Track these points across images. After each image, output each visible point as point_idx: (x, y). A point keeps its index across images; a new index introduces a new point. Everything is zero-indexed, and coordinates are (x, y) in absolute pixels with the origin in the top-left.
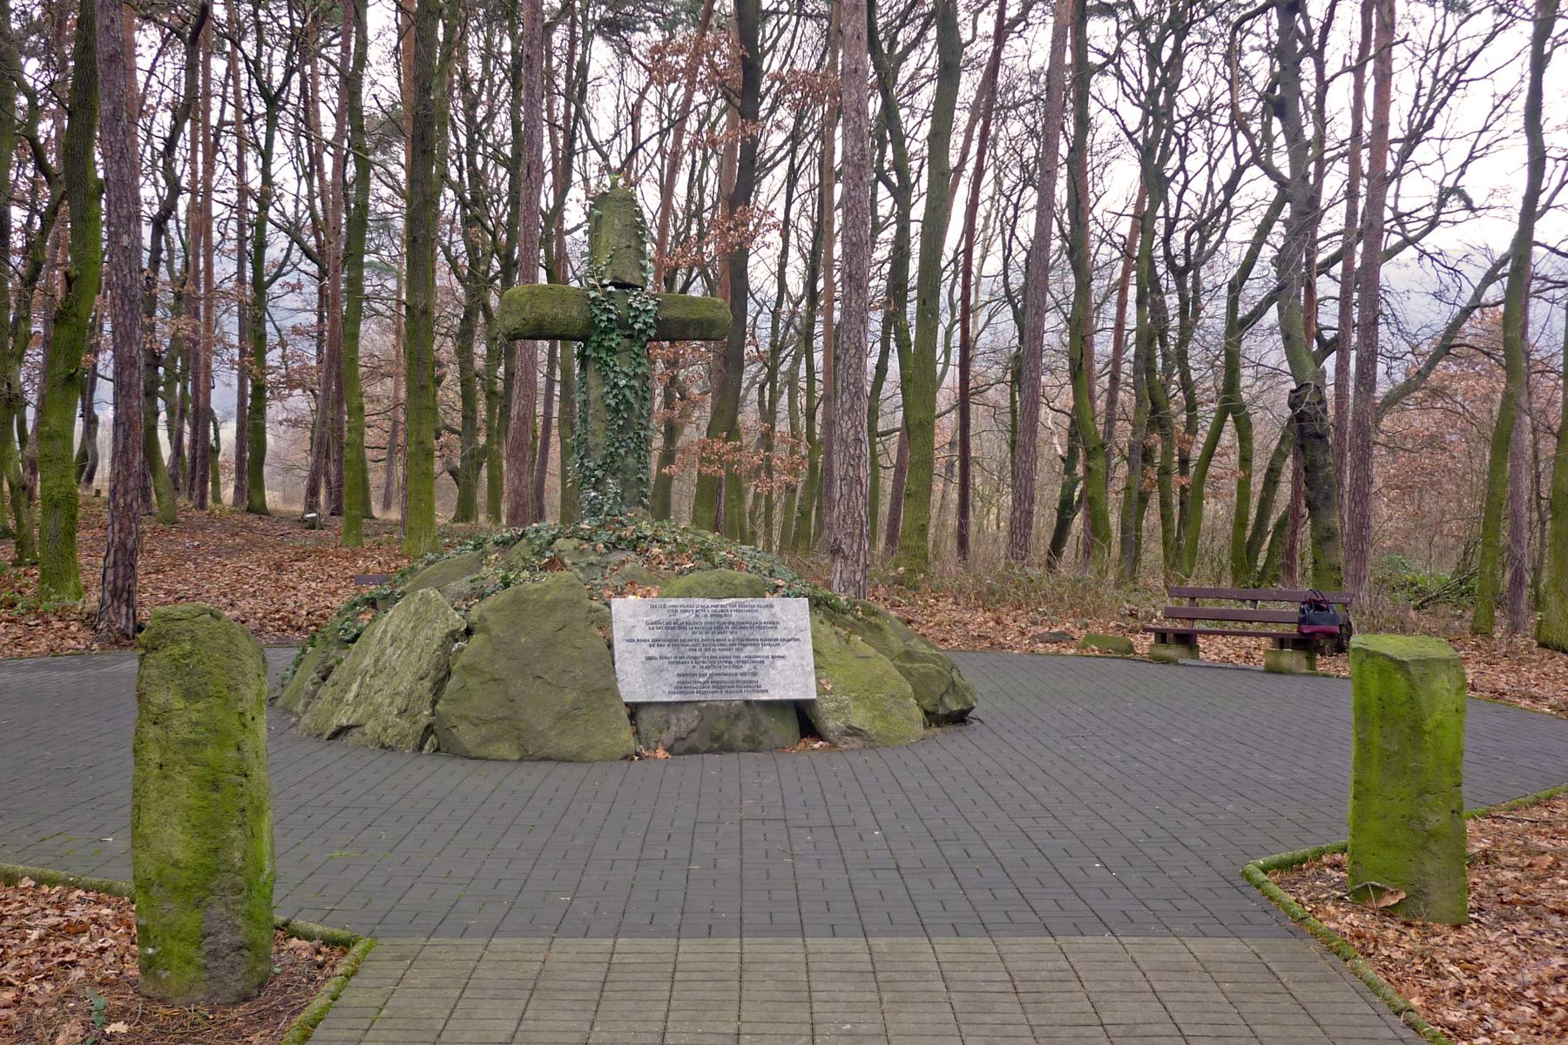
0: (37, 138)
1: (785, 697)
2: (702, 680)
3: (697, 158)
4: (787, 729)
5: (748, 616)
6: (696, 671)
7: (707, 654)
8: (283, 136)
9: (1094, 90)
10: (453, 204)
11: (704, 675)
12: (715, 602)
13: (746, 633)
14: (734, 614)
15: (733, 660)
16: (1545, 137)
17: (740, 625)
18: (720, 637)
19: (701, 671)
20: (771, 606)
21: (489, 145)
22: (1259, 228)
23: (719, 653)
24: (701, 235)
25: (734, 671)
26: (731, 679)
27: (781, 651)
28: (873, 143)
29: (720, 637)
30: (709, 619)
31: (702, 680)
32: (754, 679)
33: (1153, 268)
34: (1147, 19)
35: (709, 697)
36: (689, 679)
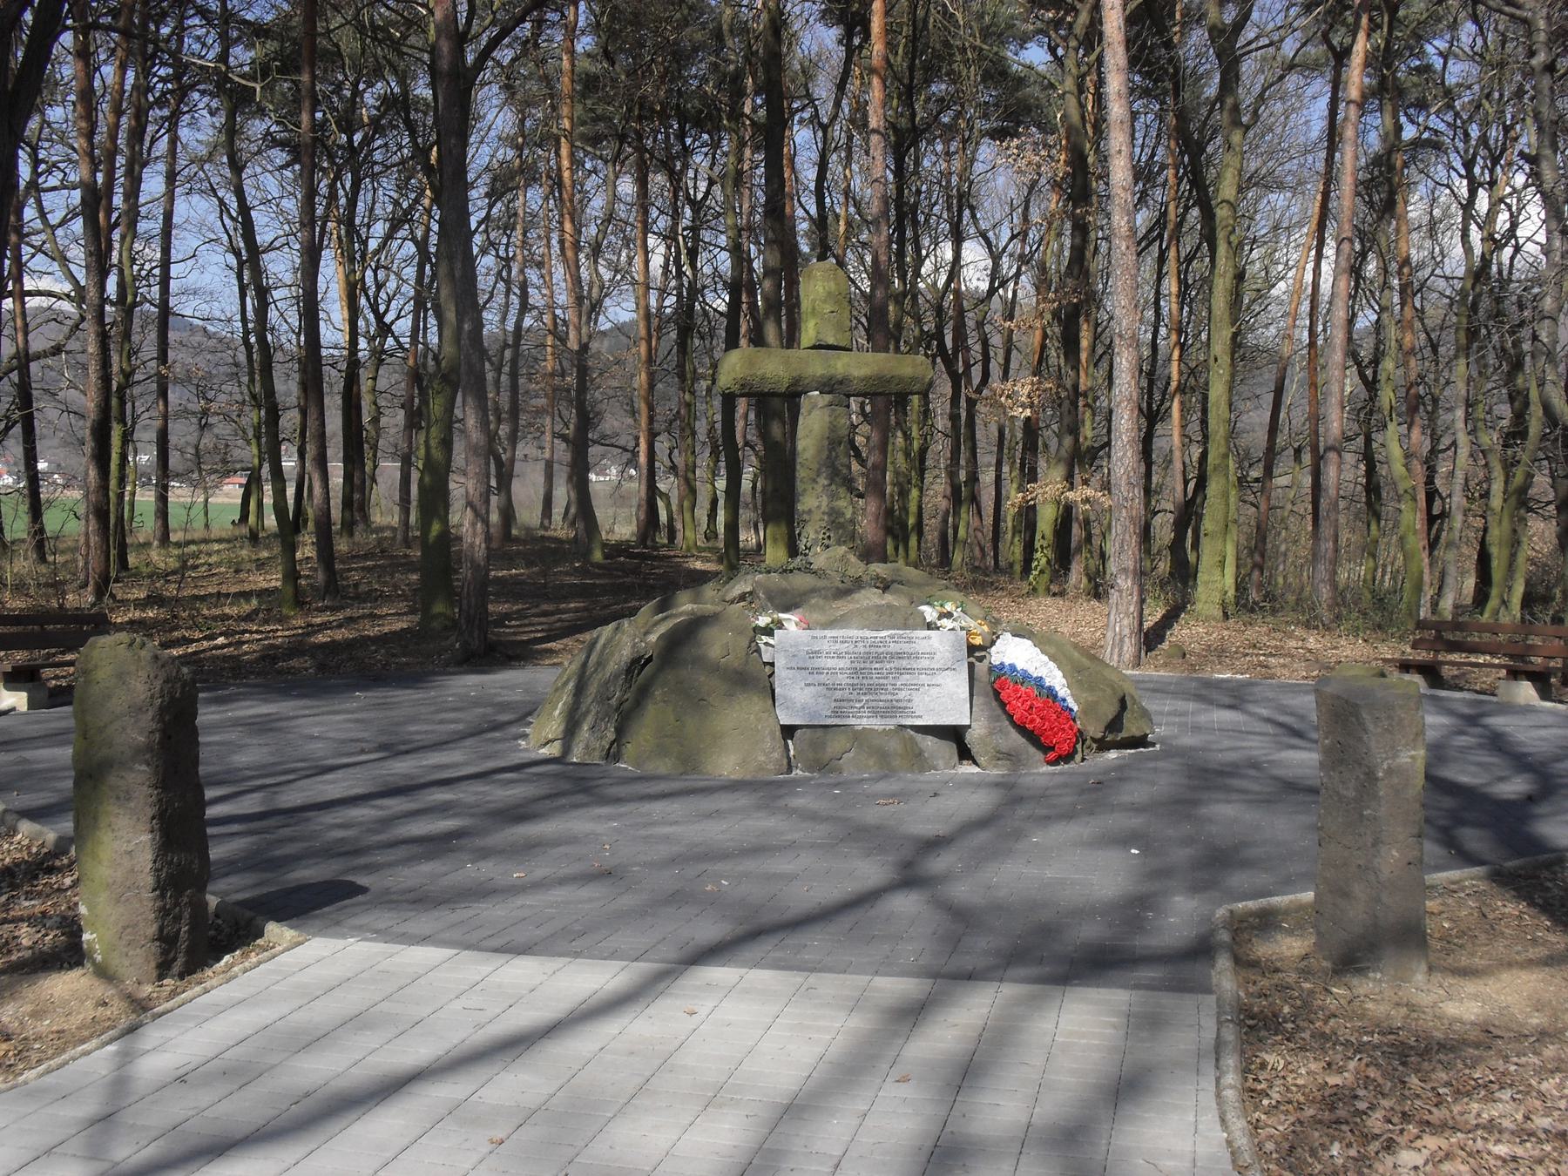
3: (267, 228)
5: (905, 647)
6: (852, 697)
7: (865, 681)
8: (807, 212)
11: (860, 701)
12: (874, 634)
13: (904, 663)
15: (889, 687)
16: (258, 238)
18: (877, 666)
22: (1327, 160)
24: (1489, 333)
25: (890, 697)
26: (887, 704)
27: (938, 679)
29: (877, 666)
30: (868, 650)
35: (864, 721)
36: (842, 704)
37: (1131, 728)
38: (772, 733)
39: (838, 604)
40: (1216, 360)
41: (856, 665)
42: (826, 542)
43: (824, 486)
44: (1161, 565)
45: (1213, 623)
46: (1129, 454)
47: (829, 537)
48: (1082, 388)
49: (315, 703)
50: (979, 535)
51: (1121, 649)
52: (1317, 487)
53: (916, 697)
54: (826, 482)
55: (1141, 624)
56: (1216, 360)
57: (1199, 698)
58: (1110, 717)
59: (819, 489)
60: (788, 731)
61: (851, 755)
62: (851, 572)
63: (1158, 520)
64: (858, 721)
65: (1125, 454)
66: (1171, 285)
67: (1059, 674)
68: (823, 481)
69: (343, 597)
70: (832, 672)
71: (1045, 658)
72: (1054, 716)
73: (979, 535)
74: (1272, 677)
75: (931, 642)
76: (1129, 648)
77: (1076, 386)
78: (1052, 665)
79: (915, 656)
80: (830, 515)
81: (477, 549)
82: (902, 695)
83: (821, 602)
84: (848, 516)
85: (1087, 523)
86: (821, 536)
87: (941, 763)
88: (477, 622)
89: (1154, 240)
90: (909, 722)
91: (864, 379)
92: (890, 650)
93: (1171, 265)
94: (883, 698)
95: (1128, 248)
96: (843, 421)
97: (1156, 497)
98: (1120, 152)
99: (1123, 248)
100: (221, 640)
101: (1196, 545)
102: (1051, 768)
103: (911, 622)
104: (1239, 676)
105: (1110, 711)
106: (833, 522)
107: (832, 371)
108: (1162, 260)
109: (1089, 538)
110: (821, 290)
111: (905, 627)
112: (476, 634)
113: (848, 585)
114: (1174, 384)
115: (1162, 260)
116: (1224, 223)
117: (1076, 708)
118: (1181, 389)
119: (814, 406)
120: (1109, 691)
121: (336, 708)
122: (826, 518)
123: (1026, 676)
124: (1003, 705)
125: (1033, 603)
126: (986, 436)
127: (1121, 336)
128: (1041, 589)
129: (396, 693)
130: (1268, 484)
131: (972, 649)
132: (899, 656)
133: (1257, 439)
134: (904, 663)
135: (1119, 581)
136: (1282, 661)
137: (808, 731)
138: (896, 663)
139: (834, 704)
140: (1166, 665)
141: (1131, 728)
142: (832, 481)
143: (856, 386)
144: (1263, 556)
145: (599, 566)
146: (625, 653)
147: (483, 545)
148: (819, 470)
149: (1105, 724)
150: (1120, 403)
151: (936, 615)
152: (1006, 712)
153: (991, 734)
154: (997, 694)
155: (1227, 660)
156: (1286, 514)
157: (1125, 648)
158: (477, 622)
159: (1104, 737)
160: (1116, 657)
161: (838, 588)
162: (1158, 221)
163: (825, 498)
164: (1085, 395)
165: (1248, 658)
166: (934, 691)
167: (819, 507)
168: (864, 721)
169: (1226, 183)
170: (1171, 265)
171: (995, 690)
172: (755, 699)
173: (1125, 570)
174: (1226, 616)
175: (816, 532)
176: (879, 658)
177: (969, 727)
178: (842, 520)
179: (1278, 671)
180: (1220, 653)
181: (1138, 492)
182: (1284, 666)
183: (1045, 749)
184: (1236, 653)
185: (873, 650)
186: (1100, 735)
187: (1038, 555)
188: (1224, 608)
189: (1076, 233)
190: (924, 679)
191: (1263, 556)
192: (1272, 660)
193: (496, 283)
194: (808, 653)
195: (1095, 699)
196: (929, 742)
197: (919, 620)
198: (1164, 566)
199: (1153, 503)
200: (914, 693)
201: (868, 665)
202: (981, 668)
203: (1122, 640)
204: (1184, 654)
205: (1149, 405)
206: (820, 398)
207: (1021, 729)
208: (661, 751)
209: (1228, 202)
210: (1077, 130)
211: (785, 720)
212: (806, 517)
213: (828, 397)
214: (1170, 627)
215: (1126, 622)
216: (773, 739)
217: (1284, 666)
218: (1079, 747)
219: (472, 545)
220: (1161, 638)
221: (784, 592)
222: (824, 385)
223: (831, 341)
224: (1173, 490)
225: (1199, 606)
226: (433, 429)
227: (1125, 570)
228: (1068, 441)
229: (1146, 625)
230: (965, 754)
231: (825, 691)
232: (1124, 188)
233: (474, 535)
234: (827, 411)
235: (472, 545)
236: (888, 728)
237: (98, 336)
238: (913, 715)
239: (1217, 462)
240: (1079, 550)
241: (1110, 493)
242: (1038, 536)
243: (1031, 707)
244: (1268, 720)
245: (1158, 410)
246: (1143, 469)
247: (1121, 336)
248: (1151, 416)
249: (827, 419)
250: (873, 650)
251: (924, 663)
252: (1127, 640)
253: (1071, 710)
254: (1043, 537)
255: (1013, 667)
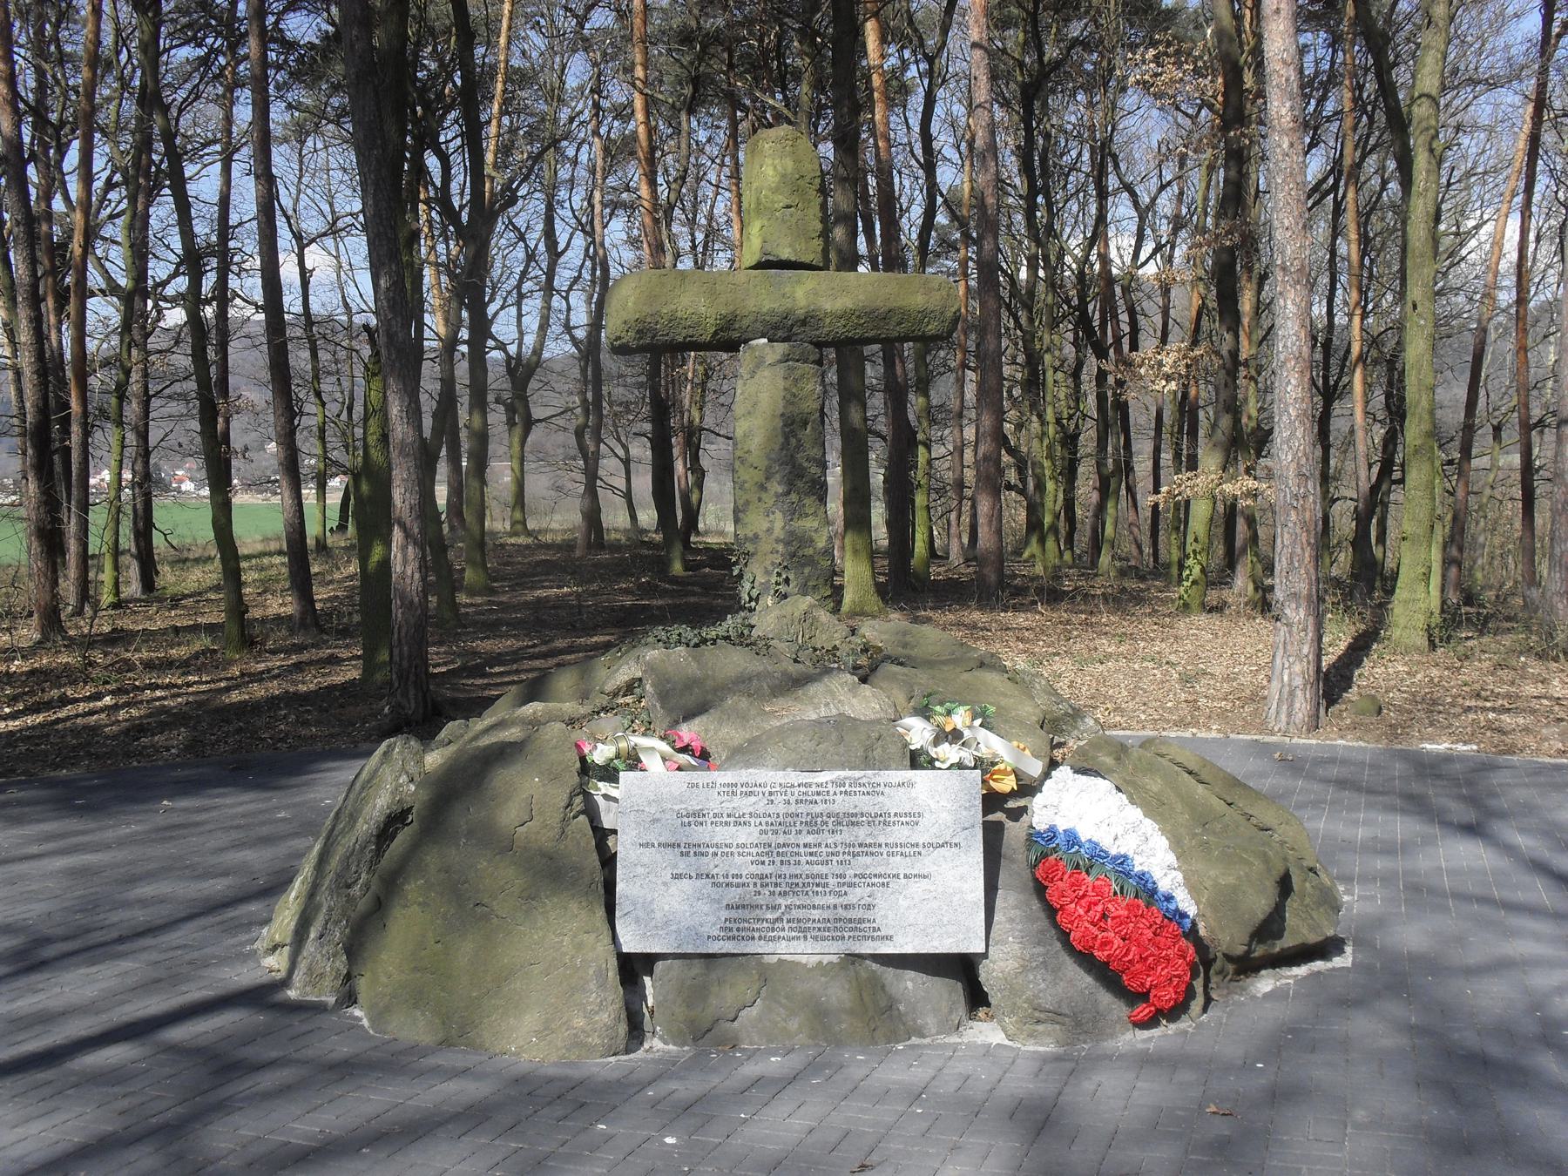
0: (1375, 21)
2: (769, 916)
4: (945, 992)
5: (865, 804)
6: (760, 900)
7: (785, 870)
9: (88, 306)
10: (105, 159)
11: (775, 908)
13: (862, 833)
14: (839, 798)
15: (832, 881)
17: (852, 820)
18: (810, 839)
23: (807, 869)
25: (831, 900)
27: (925, 864)
28: (1382, 169)
29: (810, 839)
30: (792, 809)
32: (868, 915)
33: (303, 698)
35: (782, 947)
36: (746, 914)
37: (1299, 929)
38: (601, 975)
39: (780, 703)
40: (1415, 307)
42: (782, 588)
43: (777, 495)
44: (1342, 557)
45: (1416, 657)
46: (1299, 434)
47: (787, 581)
48: (1243, 356)
49: (92, 825)
50: (1135, 530)
51: (1291, 705)
52: (1528, 469)
53: (883, 900)
54: (780, 489)
55: (1319, 661)
56: (1415, 307)
57: (1416, 805)
58: (1261, 916)
59: (769, 499)
60: (633, 968)
61: (754, 1012)
62: (821, 640)
63: (1337, 507)
65: (1293, 434)
66: (1348, 248)
67: (1161, 843)
68: (776, 487)
69: (322, 631)
70: (725, 850)
71: (1136, 813)
72: (1149, 934)
73: (1135, 530)
74: (1511, 751)
75: (914, 793)
76: (1302, 705)
77: (1234, 354)
78: (1149, 825)
79: (881, 819)
80: (787, 543)
81: (408, 581)
82: (857, 895)
83: (744, 703)
84: (821, 544)
85: (1251, 521)
86: (774, 579)
87: (930, 1022)
88: (412, 678)
89: (1327, 193)
90: (867, 948)
91: (846, 315)
92: (836, 808)
93: (1349, 219)
94: (818, 901)
95: (1292, 145)
96: (810, 387)
97: (1334, 484)
98: (1278, 11)
99: (1285, 145)
100: (108, 700)
101: (1382, 538)
102: (1146, 1034)
103: (877, 753)
104: (1461, 747)
105: (1260, 904)
106: (793, 555)
107: (787, 304)
108: (1338, 210)
109: (1254, 538)
110: (770, 172)
111: (867, 763)
112: (412, 692)
113: (806, 667)
114: (1356, 349)
115: (1338, 210)
116: (1424, 124)
117: (1191, 910)
118: (1362, 358)
119: (759, 363)
120: (1258, 865)
121: (109, 835)
122: (780, 548)
123: (1097, 855)
124: (1051, 912)
125: (1182, 625)
126: (1140, 418)
127: (1284, 269)
128: (1195, 604)
129: (228, 801)
130: (1465, 466)
131: (992, 800)
132: (852, 820)
133: (1453, 417)
134: (862, 833)
135: (1287, 611)
136: (1521, 721)
137: (677, 962)
138: (847, 835)
139: (724, 914)
140: (1354, 727)
141: (1299, 929)
142: (791, 486)
143: (825, 330)
144: (1461, 549)
145: (675, 580)
146: (380, 804)
147: (417, 576)
148: (768, 468)
149: (1250, 929)
150: (1284, 363)
152: (1055, 925)
153: (1025, 969)
154: (1040, 890)
155: (1441, 718)
156: (1485, 500)
157: (1297, 705)
158: (412, 678)
159: (1249, 952)
160: (1283, 717)
161: (784, 673)
162: (1332, 171)
163: (779, 515)
164: (1246, 364)
165: (1472, 716)
166: (917, 887)
167: (769, 531)
168: (782, 947)
169: (1426, 71)
170: (1349, 219)
171: (1036, 880)
172: (574, 906)
173: (1295, 596)
174: (1433, 646)
175: (767, 573)
176: (813, 824)
177: (985, 955)
178: (810, 551)
179: (1520, 739)
180: (1430, 707)
181: (1313, 486)
182: (1526, 730)
183: (1133, 997)
184: (1453, 705)
185: (802, 809)
186: (1240, 950)
187: (1190, 562)
188: (1430, 636)
189: (1231, 164)
190: (898, 864)
191: (1461, 549)
192: (1506, 718)
193: (584, 261)
194: (679, 815)
195: (1231, 880)
196: (910, 983)
197: (894, 749)
198: (1342, 564)
199: (1331, 490)
200: (878, 891)
201: (792, 839)
202: (1014, 832)
203: (1292, 693)
204: (1380, 708)
205: (1326, 378)
206: (768, 350)
207: (1085, 959)
208: (417, 998)
209: (1428, 96)
210: (1231, 40)
211: (631, 943)
212: (750, 547)
213: (781, 348)
214: (1359, 664)
215: (1297, 668)
216: (602, 986)
217: (1526, 730)
218: (1198, 985)
219: (403, 576)
220: (1347, 682)
221: (691, 684)
222: (776, 327)
223: (786, 254)
224: (1357, 476)
225: (1396, 633)
226: (371, 421)
227: (1295, 596)
228: (1225, 422)
229: (1326, 661)
230: (977, 999)
231: (709, 889)
232: (1284, 62)
233: (405, 562)
234: (780, 370)
235: (403, 576)
236: (826, 959)
237: (31, 321)
238: (875, 934)
239: (1418, 442)
240: (1244, 551)
242: (1190, 539)
243: (1104, 916)
244: (1540, 867)
245: (1337, 382)
246: (1319, 452)
247: (1284, 269)
248: (1328, 392)
249: (781, 384)
250: (802, 809)
251: (899, 834)
252: (1299, 693)
253: (1184, 915)
254: (1196, 540)
255: (1072, 839)
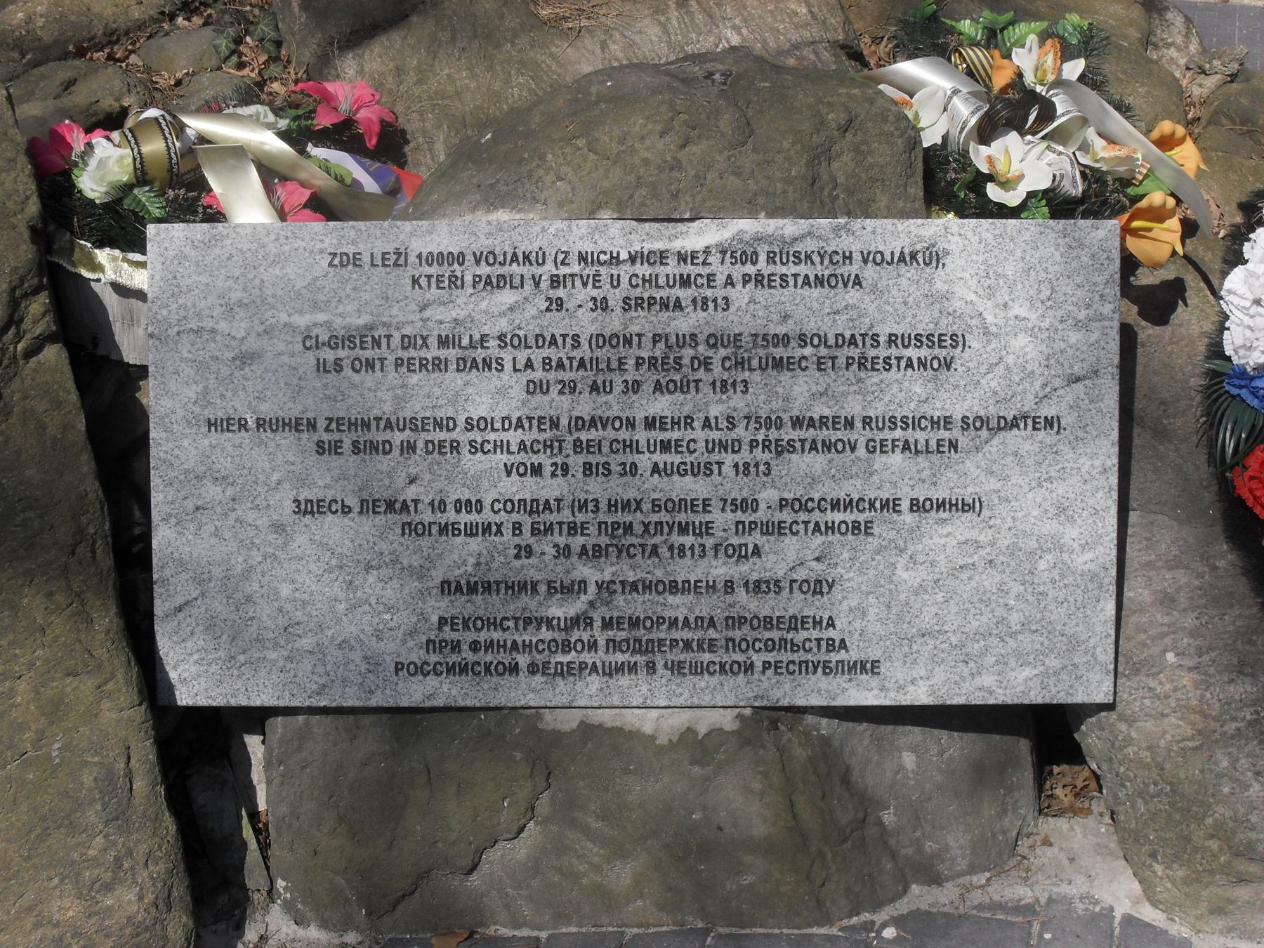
1: (884, 704)
2: (559, 610)
6: (530, 569)
7: (596, 488)
11: (573, 589)
14: (740, 295)
15: (721, 519)
18: (662, 405)
19: (557, 570)
20: (932, 257)
21: (41, 281)
25: (720, 569)
26: (705, 606)
29: (662, 405)
30: (614, 322)
31: (559, 610)
34: (599, 207)
36: (494, 605)
41: (543, 404)
64: (561, 691)
75: (939, 280)
92: (718, 321)
94: (684, 570)
103: (842, 165)
151: (967, 112)
185: (642, 322)
194: (310, 342)
197: (884, 154)
200: (842, 547)
201: (613, 405)
241: (861, 287)
250: (642, 322)
